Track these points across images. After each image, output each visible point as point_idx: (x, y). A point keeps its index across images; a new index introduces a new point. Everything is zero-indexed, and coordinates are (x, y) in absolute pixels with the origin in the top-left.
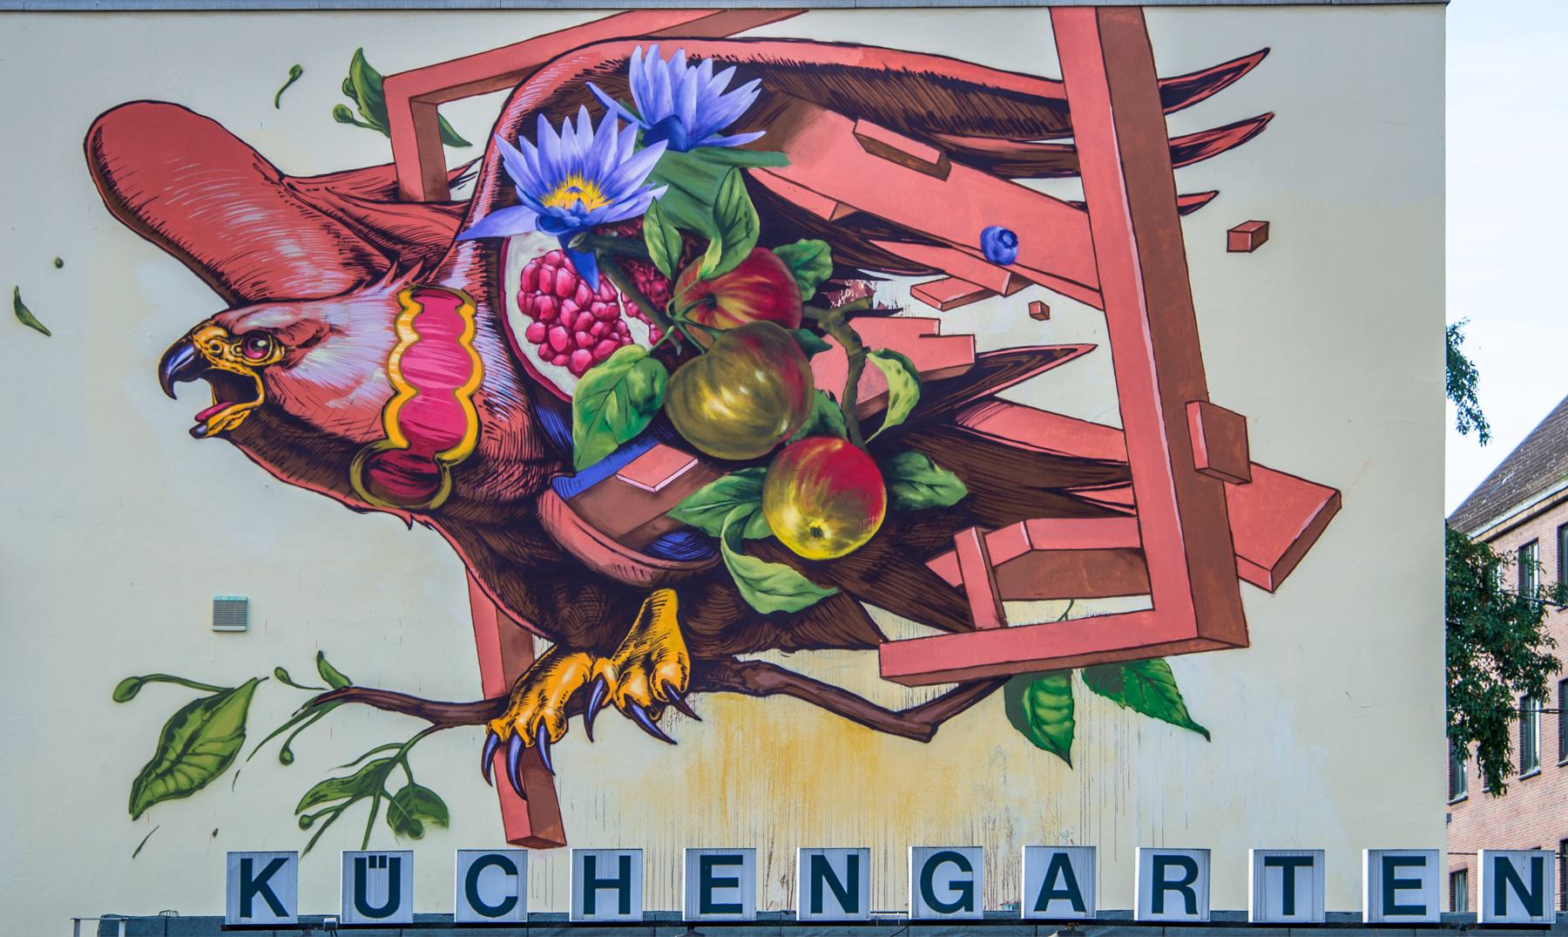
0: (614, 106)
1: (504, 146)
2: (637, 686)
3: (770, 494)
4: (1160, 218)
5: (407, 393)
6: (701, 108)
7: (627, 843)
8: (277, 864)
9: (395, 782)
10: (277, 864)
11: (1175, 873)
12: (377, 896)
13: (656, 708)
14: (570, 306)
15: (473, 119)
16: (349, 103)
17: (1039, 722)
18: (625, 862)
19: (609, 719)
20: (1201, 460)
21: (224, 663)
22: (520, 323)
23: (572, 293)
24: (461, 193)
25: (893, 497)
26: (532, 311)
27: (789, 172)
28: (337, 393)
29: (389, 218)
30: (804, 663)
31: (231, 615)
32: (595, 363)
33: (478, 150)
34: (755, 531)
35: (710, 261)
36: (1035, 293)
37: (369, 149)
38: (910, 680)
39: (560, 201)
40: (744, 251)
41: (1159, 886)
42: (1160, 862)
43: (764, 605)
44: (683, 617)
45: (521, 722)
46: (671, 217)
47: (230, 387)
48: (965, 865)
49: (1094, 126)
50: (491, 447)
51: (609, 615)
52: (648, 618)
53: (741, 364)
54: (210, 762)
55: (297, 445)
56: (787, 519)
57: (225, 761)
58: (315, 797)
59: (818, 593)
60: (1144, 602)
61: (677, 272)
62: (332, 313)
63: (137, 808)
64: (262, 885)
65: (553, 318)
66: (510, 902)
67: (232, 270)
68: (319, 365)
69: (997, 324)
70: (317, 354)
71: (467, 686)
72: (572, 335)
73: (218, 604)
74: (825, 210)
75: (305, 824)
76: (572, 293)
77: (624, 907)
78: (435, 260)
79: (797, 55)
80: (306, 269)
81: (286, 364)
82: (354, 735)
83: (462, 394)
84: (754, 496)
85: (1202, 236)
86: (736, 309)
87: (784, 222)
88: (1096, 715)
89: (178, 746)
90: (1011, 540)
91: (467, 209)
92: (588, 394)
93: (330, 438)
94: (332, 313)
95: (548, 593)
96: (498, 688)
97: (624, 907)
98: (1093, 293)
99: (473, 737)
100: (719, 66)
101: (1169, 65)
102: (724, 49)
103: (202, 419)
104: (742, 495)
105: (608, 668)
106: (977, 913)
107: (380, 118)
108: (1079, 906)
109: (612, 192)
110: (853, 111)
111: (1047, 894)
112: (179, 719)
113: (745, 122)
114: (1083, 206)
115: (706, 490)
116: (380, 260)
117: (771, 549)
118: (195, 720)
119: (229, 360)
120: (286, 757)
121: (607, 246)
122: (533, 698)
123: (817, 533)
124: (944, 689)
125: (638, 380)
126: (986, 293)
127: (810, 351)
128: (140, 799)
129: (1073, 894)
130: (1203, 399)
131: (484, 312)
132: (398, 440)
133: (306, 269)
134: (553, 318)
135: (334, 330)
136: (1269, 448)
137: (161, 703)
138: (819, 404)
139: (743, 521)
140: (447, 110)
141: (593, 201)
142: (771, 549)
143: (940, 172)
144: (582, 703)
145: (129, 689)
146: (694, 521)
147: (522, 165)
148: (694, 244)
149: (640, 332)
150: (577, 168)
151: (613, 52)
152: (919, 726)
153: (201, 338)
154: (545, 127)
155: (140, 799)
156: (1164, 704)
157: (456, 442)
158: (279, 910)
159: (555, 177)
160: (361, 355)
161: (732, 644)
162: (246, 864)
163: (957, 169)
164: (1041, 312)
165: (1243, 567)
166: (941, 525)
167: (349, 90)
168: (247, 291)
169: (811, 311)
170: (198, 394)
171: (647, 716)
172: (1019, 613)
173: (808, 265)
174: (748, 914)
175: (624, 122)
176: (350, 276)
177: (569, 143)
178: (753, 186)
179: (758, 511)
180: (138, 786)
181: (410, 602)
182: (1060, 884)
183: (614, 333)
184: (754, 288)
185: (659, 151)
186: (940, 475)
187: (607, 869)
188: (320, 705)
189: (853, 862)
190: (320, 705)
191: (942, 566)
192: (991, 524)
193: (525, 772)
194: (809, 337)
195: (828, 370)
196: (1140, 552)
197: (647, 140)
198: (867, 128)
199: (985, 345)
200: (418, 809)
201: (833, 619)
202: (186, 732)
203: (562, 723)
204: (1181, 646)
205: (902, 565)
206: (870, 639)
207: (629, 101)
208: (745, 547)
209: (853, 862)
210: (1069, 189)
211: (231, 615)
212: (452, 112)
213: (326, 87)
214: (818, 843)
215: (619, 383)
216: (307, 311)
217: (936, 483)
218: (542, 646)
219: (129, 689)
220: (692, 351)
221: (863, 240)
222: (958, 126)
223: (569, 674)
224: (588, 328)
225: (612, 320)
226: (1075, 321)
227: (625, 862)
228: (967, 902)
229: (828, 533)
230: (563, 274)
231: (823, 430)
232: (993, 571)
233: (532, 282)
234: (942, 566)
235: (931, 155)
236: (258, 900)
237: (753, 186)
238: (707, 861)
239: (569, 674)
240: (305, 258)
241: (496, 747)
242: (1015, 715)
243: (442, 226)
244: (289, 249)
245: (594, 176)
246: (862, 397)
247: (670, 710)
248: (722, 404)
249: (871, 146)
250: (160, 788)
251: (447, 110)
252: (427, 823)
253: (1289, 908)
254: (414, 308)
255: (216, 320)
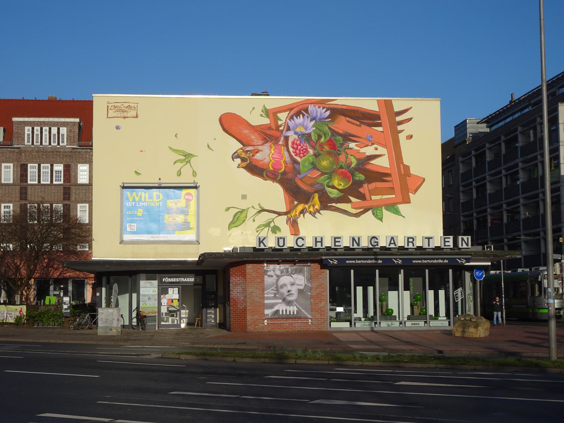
0: (306, 115)
1: (288, 121)
2: (311, 209)
3: (333, 178)
4: (396, 134)
5: (273, 161)
6: (320, 115)
7: (359, 235)
8: (265, 238)
9: (272, 225)
10: (265, 238)
11: (411, 240)
12: (281, 244)
13: (315, 213)
14: (299, 147)
15: (283, 116)
16: (263, 113)
17: (377, 215)
18: (322, 238)
19: (307, 215)
20: (403, 173)
21: (243, 205)
22: (291, 150)
23: (300, 145)
24: (281, 128)
25: (353, 178)
26: (293, 148)
27: (335, 126)
28: (261, 161)
29: (269, 132)
30: (340, 206)
31: (244, 197)
32: (304, 156)
33: (284, 121)
34: (330, 184)
35: (322, 140)
36: (375, 146)
37: (266, 121)
38: (356, 208)
39: (298, 130)
40: (328, 138)
41: (408, 242)
42: (408, 238)
43: (332, 196)
44: (319, 198)
45: (293, 215)
46: (316, 133)
47: (243, 160)
48: (377, 239)
49: (384, 119)
50: (287, 170)
51: (305, 198)
52: (313, 198)
53: (328, 157)
54: (241, 221)
55: (254, 169)
56: (336, 183)
57: (244, 221)
58: (259, 227)
59: (341, 194)
60: (394, 196)
61: (317, 141)
62: (260, 148)
63: (229, 229)
64: (262, 242)
65: (297, 149)
66: (303, 245)
67: (243, 141)
68: (258, 156)
69: (369, 151)
70: (258, 154)
71: (284, 210)
72: (300, 151)
73: (242, 195)
74: (341, 132)
75: (257, 232)
76: (300, 145)
77: (322, 246)
78: (277, 139)
79: (336, 107)
80: (256, 140)
81: (253, 156)
82: (267, 217)
83: (282, 161)
84: (330, 178)
85: (402, 137)
86: (327, 148)
87: (334, 133)
88: (386, 213)
89: (236, 219)
90: (374, 185)
91: (282, 131)
92: (302, 161)
93: (261, 168)
94: (260, 148)
95: (297, 193)
96: (288, 209)
97: (322, 246)
98: (385, 146)
99: (285, 217)
100: (323, 108)
101: (396, 109)
102: (324, 106)
103: (239, 165)
104: (328, 178)
105: (307, 206)
106: (379, 247)
107: (268, 116)
108: (395, 245)
109: (306, 128)
110: (345, 116)
111: (390, 243)
112: (236, 214)
113: (328, 118)
114: (383, 132)
115: (322, 177)
116: (268, 139)
117: (333, 187)
118: (238, 215)
119: (243, 155)
120: (254, 221)
121: (307, 137)
122: (294, 211)
123: (341, 184)
124: (362, 210)
125: (311, 159)
126: (367, 146)
127: (339, 155)
128: (230, 227)
129: (394, 243)
130: (403, 163)
131: (285, 148)
132: (271, 169)
133: (256, 140)
134: (297, 149)
135: (261, 151)
136: (412, 172)
137: (233, 212)
138: (340, 163)
139: (328, 183)
140: (279, 115)
141: (303, 130)
142: (333, 187)
143: (360, 126)
144: (302, 212)
145: (228, 209)
146: (321, 182)
147: (291, 124)
148: (320, 137)
149: (311, 151)
150: (300, 125)
151: (306, 106)
152: (357, 215)
153: (239, 152)
154: (295, 117)
155: (230, 227)
156: (397, 212)
157: (281, 169)
158: (265, 246)
159: (297, 126)
160: (266, 154)
161: (326, 203)
162: (260, 238)
163: (362, 125)
164: (376, 149)
165: (410, 190)
166: (360, 184)
167: (262, 111)
168: (246, 144)
169: (339, 148)
170: (238, 161)
171: (313, 214)
172: (374, 198)
173: (338, 141)
174: (342, 247)
175: (308, 117)
176: (262, 142)
177: (299, 120)
178: (330, 128)
179: (331, 181)
180: (229, 225)
181: (274, 194)
182: (392, 242)
183: (306, 151)
184: (329, 144)
185: (313, 122)
186: (360, 175)
187: (319, 240)
188: (259, 212)
189: (359, 238)
190: (259, 212)
191: (361, 190)
192: (369, 182)
193: (294, 225)
194: (339, 152)
195: (342, 158)
196: (393, 188)
197: (311, 120)
198: (347, 119)
199: (367, 154)
200: (275, 229)
201: (344, 199)
202: (237, 216)
203: (299, 215)
204: (400, 203)
205: (353, 191)
206: (349, 201)
207: (308, 114)
208: (329, 187)
209: (359, 238)
210: (380, 129)
211: (244, 197)
212: (279, 115)
213: (259, 110)
214: (353, 235)
215: (308, 159)
216: (256, 147)
217: (360, 177)
218: (296, 203)
219: (228, 209)
220: (319, 155)
221: (348, 137)
222: (363, 119)
223: (300, 207)
224: (302, 151)
225: (306, 149)
226: (382, 150)
227: (322, 238)
228: (377, 245)
229: (342, 184)
230: (298, 142)
231: (341, 167)
232: (369, 191)
233: (293, 143)
234: (361, 190)
235: (358, 123)
236: (262, 244)
237: (330, 128)
238: (335, 238)
239: (300, 207)
240: (255, 138)
241: (288, 220)
242: (373, 214)
243: (278, 134)
244: (253, 137)
245: (303, 126)
246: (348, 162)
247: (317, 213)
248: (325, 163)
249: (348, 122)
250: (233, 225)
251: (279, 115)
252: (277, 231)
253: (429, 246)
254: (274, 147)
255: (241, 149)
